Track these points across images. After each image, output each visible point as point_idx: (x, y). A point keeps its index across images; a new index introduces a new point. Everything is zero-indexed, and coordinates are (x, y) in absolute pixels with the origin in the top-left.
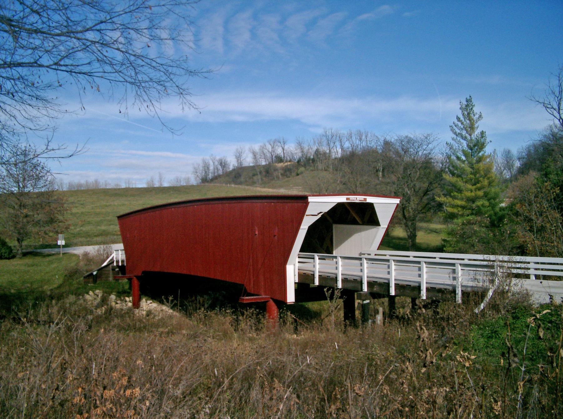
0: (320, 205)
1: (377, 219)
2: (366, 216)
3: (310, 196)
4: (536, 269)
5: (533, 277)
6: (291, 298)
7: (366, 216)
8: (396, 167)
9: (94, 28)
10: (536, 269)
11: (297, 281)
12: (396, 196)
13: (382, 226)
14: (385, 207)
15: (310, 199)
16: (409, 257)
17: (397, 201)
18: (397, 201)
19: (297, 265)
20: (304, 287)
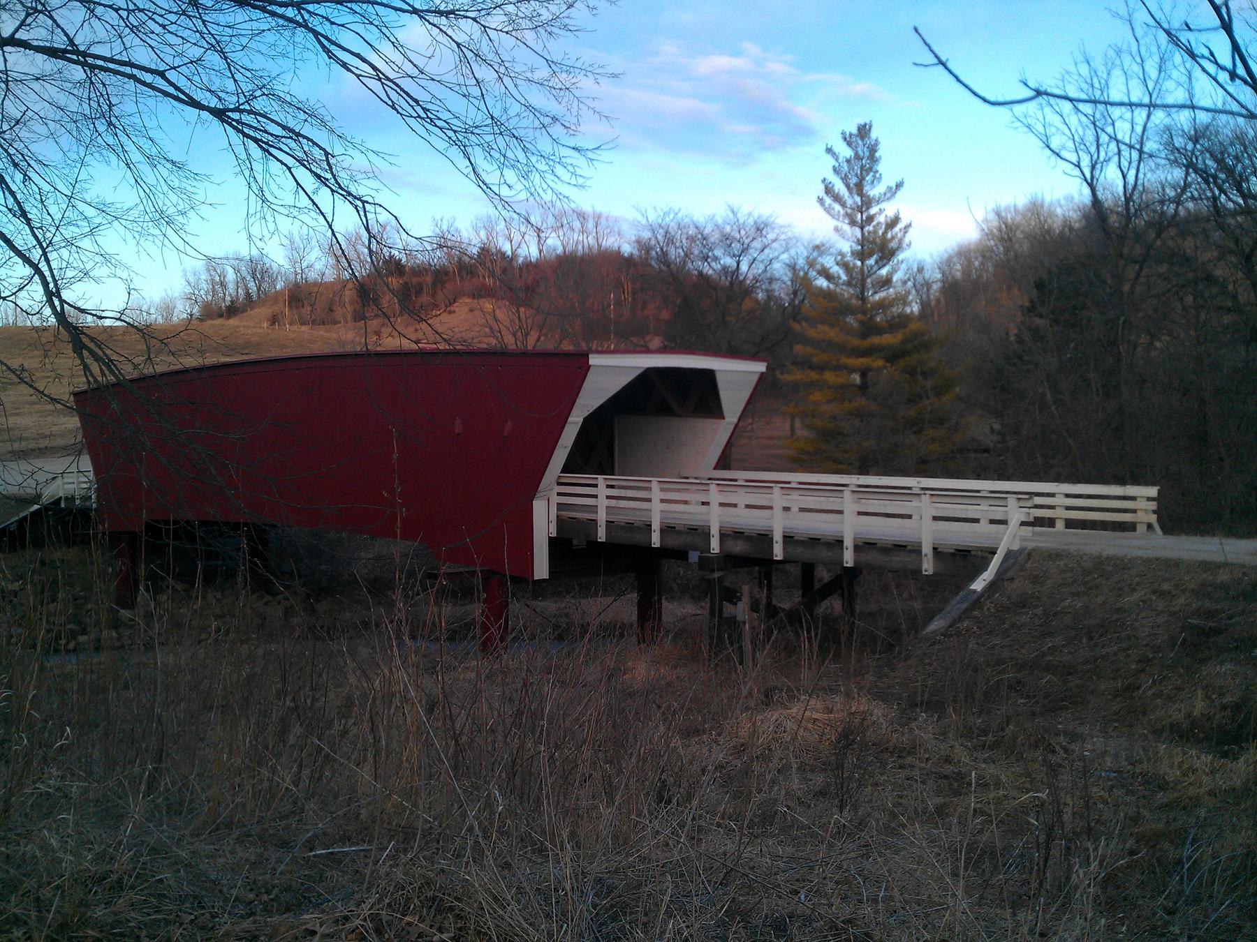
0: (610, 371)
1: (618, 392)
2: (698, 394)
3: (593, 352)
4: (1068, 508)
5: (1060, 525)
6: (541, 569)
7: (698, 394)
8: (180, 218)
9: (1088, 176)
10: (1068, 508)
11: (554, 535)
12: (754, 357)
13: (728, 419)
14: (736, 375)
15: (594, 360)
16: (1052, 495)
17: (761, 367)
18: (761, 367)
19: (556, 499)
20: (573, 548)
